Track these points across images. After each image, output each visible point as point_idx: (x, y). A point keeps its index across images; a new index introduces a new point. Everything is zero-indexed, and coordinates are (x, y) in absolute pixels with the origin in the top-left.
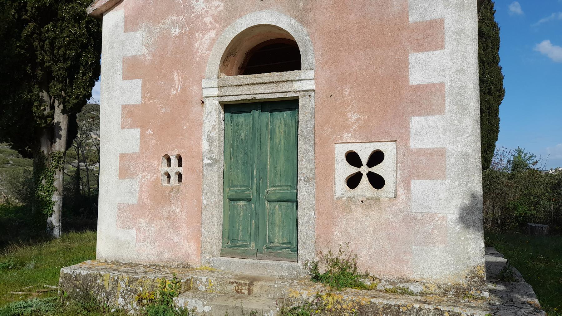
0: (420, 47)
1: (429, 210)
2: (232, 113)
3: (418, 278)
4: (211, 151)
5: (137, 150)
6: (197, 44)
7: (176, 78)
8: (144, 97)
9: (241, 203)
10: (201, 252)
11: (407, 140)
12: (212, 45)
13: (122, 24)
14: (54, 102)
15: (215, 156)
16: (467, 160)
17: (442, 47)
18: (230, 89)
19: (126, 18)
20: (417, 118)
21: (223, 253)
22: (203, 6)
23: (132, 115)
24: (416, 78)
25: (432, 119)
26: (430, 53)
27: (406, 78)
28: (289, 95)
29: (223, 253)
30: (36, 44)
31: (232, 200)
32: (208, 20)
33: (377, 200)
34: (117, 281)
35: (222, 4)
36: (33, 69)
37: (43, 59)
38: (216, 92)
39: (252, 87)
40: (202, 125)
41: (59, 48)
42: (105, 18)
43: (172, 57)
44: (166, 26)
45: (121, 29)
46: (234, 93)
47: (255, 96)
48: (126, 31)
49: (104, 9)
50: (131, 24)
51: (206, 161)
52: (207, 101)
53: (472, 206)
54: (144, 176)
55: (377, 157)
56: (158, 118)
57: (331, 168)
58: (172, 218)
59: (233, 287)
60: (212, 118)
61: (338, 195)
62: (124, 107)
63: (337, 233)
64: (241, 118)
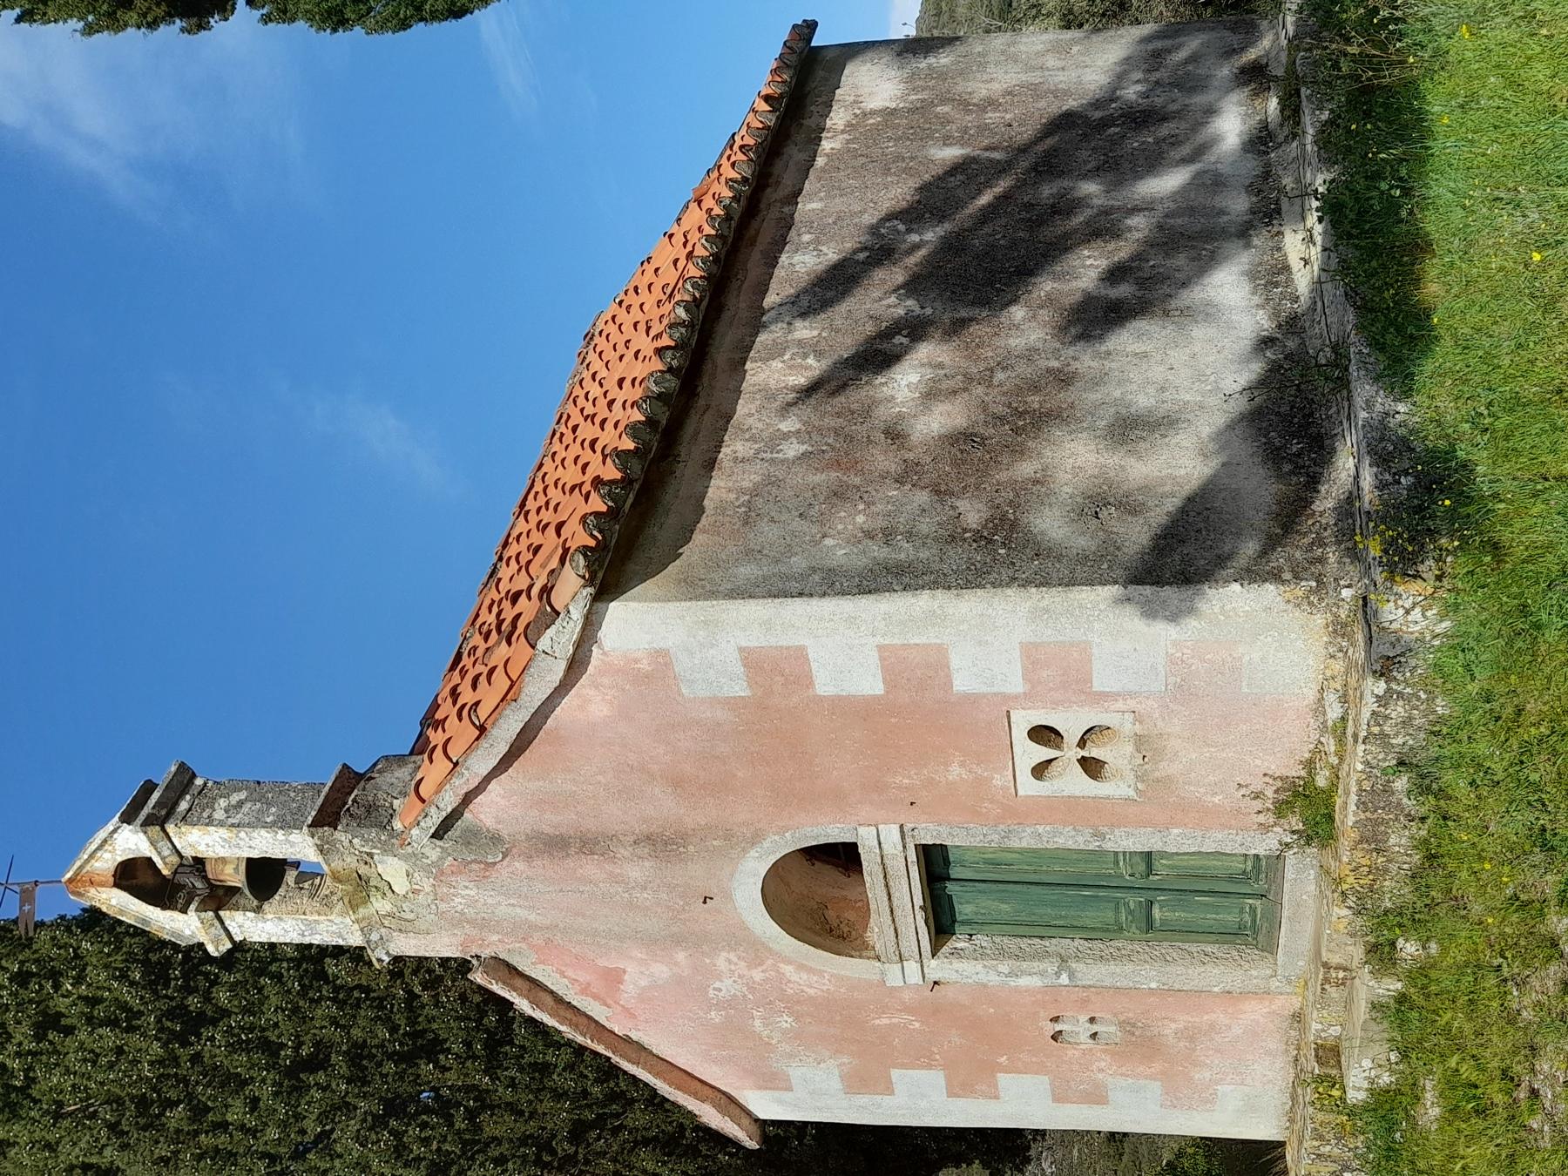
0: (804, 679)
1: (1160, 668)
2: (954, 921)
4: (1042, 974)
6: (811, 992)
8: (929, 1067)
9: (1157, 913)
11: (1006, 698)
13: (777, 1094)
18: (904, 944)
19: (760, 1088)
20: (955, 683)
21: (1270, 948)
24: (870, 683)
25: (955, 661)
26: (814, 666)
28: (912, 857)
31: (1150, 925)
32: (757, 975)
34: (1318, 1155)
35: (724, 954)
38: (912, 967)
39: (897, 912)
40: (985, 986)
42: (762, 1116)
45: (787, 1096)
47: (917, 907)
48: (790, 1089)
49: (746, 1121)
50: (773, 1081)
52: (933, 975)
54: (1101, 1070)
55: (1044, 734)
56: (981, 1044)
58: (1191, 1036)
59: (1332, 991)
60: (966, 969)
61: (1132, 793)
62: (951, 1094)
64: (964, 910)
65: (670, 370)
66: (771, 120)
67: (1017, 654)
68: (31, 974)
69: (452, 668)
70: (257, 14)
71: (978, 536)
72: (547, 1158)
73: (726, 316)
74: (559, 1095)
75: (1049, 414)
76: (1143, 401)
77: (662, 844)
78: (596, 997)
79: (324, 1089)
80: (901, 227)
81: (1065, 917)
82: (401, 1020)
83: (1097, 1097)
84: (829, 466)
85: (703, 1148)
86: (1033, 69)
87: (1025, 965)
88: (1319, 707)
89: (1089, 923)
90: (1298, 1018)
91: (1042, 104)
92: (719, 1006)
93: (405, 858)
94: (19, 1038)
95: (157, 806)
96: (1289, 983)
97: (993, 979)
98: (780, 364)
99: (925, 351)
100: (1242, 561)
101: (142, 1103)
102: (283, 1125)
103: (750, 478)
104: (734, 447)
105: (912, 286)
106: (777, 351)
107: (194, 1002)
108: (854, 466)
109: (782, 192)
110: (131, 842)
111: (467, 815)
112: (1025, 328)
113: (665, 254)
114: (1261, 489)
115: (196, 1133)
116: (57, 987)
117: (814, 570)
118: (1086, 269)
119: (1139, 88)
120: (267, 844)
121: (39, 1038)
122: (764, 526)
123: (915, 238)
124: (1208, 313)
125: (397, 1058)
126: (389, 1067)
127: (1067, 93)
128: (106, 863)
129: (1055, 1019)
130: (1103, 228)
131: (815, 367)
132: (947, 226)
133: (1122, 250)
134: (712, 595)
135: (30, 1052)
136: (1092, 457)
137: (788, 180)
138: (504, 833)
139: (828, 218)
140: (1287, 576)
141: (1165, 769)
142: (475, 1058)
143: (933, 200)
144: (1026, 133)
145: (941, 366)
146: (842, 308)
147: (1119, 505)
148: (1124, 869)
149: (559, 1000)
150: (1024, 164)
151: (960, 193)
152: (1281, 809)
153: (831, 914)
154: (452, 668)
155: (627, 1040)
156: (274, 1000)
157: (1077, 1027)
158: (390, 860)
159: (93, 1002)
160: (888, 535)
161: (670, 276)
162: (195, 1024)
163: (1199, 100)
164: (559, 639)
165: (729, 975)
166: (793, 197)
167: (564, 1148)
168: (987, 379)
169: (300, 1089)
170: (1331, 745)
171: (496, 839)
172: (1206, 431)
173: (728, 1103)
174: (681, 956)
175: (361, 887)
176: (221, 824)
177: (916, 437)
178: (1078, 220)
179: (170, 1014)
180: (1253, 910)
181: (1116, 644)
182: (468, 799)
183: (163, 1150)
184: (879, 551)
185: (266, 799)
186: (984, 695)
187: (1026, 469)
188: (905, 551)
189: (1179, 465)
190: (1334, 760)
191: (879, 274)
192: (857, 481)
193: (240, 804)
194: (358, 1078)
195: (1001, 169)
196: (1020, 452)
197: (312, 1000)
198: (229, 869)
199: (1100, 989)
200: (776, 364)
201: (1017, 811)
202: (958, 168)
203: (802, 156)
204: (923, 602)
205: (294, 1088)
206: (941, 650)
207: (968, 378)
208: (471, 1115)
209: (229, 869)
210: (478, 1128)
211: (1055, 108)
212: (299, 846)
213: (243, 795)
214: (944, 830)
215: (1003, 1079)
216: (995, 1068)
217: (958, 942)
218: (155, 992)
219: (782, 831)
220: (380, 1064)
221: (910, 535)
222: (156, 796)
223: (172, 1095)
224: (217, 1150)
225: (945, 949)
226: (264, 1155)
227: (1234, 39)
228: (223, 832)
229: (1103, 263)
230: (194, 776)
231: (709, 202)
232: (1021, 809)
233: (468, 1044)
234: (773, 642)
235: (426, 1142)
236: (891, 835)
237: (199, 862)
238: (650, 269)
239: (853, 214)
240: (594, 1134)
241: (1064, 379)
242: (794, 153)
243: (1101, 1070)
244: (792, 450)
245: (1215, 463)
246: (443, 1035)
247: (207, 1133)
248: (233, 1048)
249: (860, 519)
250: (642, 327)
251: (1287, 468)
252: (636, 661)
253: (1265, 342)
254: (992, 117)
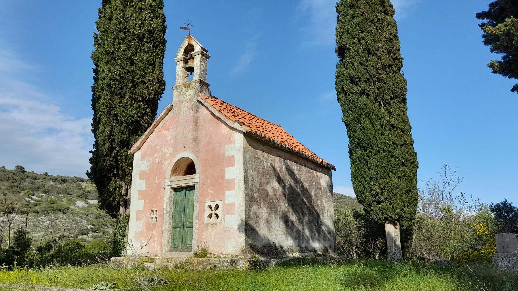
4: (167, 208)
5: (142, 209)
8: (146, 187)
9: (178, 229)
11: (224, 200)
12: (169, 165)
15: (168, 210)
17: (234, 166)
21: (171, 250)
23: (142, 195)
24: (228, 177)
25: (231, 191)
27: (224, 176)
28: (192, 184)
29: (171, 250)
30: (119, 158)
31: (175, 228)
32: (168, 155)
36: (118, 171)
38: (169, 184)
41: (129, 160)
45: (140, 159)
48: (141, 160)
50: (143, 157)
51: (165, 212)
52: (166, 188)
53: (242, 223)
55: (217, 207)
56: (151, 196)
57: (203, 212)
60: (168, 194)
62: (139, 191)
64: (179, 193)
68: (152, 7)
70: (338, 62)
71: (252, 196)
74: (123, 112)
76: (272, 225)
77: (196, 140)
78: (163, 125)
82: (140, 80)
83: (138, 219)
88: (222, 254)
89: (176, 216)
92: (161, 148)
93: (194, 95)
95: (204, 54)
97: (166, 199)
98: (278, 162)
99: (280, 189)
101: (125, 28)
102: (119, 56)
103: (261, 158)
104: (266, 155)
105: (291, 186)
106: (281, 162)
109: (306, 164)
110: (198, 49)
112: (284, 206)
113: (294, 141)
114: (259, 244)
115: (118, 39)
116: (149, 13)
118: (293, 217)
120: (197, 71)
121: (139, 9)
124: (286, 238)
129: (156, 211)
130: (300, 220)
131: (278, 169)
132: (300, 193)
134: (244, 151)
137: (308, 165)
139: (302, 172)
141: (210, 229)
142: (132, 95)
143: (305, 191)
144: (316, 208)
146: (287, 174)
149: (163, 119)
152: (202, 249)
153: (178, 169)
155: (153, 131)
156: (146, 56)
158: (193, 92)
159: (145, 19)
161: (291, 143)
162: (141, 40)
164: (237, 126)
165: (167, 150)
166: (305, 166)
167: (113, 112)
168: (276, 199)
169: (127, 60)
170: (216, 256)
171: (197, 111)
172: (268, 236)
173: (139, 149)
175: (188, 86)
177: (267, 186)
181: (234, 219)
182: (205, 106)
183: (115, 32)
184: (250, 179)
185: (204, 71)
187: (262, 205)
188: (250, 183)
189: (262, 231)
191: (293, 181)
194: (128, 72)
196: (265, 204)
200: (279, 162)
201: (202, 202)
202: (310, 196)
204: (243, 186)
205: (127, 59)
206: (234, 189)
207: (276, 195)
208: (120, 94)
211: (320, 214)
212: (196, 76)
215: (143, 201)
217: (173, 192)
221: (252, 184)
224: (115, 42)
226: (113, 51)
227: (332, 248)
231: (304, 150)
232: (201, 204)
233: (135, 94)
234: (236, 161)
235: (115, 85)
236: (197, 180)
237: (193, 58)
238: (291, 138)
241: (276, 212)
242: (313, 166)
244: (265, 165)
245: (263, 237)
248: (136, 47)
253: (282, 247)
254: (319, 202)
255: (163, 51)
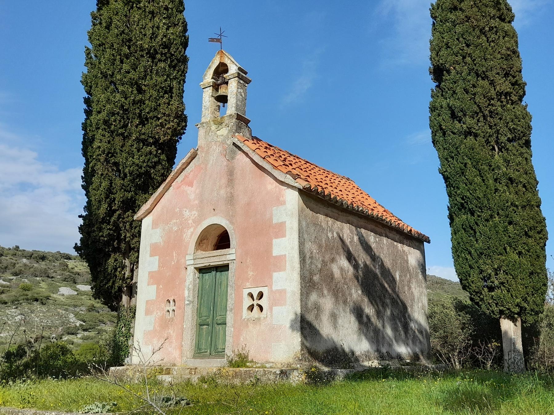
0: (277, 237)
3: (273, 361)
4: (189, 297)
6: (185, 236)
7: (174, 255)
8: (159, 266)
9: (205, 327)
10: (182, 355)
11: (271, 286)
12: (192, 236)
13: (151, 225)
14: (133, 267)
15: (191, 299)
16: (295, 295)
18: (199, 260)
19: (153, 221)
21: (194, 357)
22: (188, 214)
23: (154, 278)
24: (276, 252)
25: (282, 273)
26: (281, 239)
27: (271, 252)
28: (225, 262)
29: (194, 357)
30: (121, 225)
31: (201, 325)
32: (190, 222)
33: (259, 319)
36: (119, 243)
37: (125, 236)
38: (192, 262)
39: (209, 258)
43: (173, 243)
44: (171, 226)
45: (150, 227)
46: (218, 260)
48: (152, 228)
49: (142, 216)
50: (155, 225)
51: (187, 302)
52: (188, 268)
53: (296, 319)
54: (157, 313)
55: (261, 295)
56: (166, 280)
59: (188, 371)
60: (190, 277)
61: (244, 318)
62: (149, 273)
63: (242, 339)
64: (207, 276)
65: (348, 206)
66: (405, 231)
67: (283, 288)
68: (168, 10)
69: (269, 145)
71: (311, 279)
72: (110, 155)
73: (359, 219)
74: (127, 159)
75: (337, 298)
76: (340, 321)
77: (231, 200)
78: (184, 179)
79: (132, 92)
80: (380, 264)
81: (204, 302)
82: (151, 114)
83: (148, 312)
84: (326, 244)
85: (108, 200)
86: (418, 300)
87: (191, 292)
89: (202, 309)
90: (174, 365)
91: (409, 301)
94: (149, 6)
96: (185, 362)
97: (187, 283)
98: (348, 232)
99: (351, 269)
100: (305, 342)
101: (130, 40)
102: (121, 80)
105: (366, 265)
106: (351, 231)
107: (158, 56)
108: (326, 250)
109: (388, 233)
110: (233, 69)
111: (240, 152)
112: (356, 294)
113: (371, 201)
114: (321, 349)
115: (120, 55)
116: (164, 18)
117: (304, 240)
118: (369, 310)
119: (413, 327)
122: (314, 228)
123: (377, 267)
124: (360, 340)
125: (140, 114)
126: (138, 111)
127: (412, 308)
128: (227, 61)
129: (174, 301)
130: (379, 314)
132: (380, 275)
133: (374, 319)
134: (299, 216)
135: (145, 9)
136: (328, 308)
137: (391, 235)
138: (234, 160)
140: (302, 352)
141: (251, 326)
142: (140, 135)
143: (387, 273)
144: (402, 297)
145: (348, 272)
147: (317, 314)
148: (218, 318)
149: (183, 169)
150: (395, 296)
151: (388, 279)
152: (240, 355)
153: (205, 241)
154: (269, 145)
155: (170, 186)
157: (171, 307)
159: (158, 28)
160: (311, 258)
162: (153, 57)
163: (410, 342)
164: (289, 179)
165: (190, 214)
166: (387, 236)
167: (112, 160)
169: (132, 85)
170: (259, 365)
171: (233, 158)
173: (149, 212)
174: (197, 202)
175: (219, 123)
176: (237, 91)
178: (381, 308)
179: (155, 50)
180: (206, 352)
181: (284, 312)
182: (244, 152)
183: (115, 46)
184: (308, 255)
185: (243, 102)
186: (272, 280)
187: (325, 292)
188: (308, 261)
189: (326, 329)
190: (255, 366)
191: (369, 258)
192: (323, 251)
193: (241, 95)
195: (394, 290)
196: (329, 291)
197: (159, 90)
198: (224, 90)
199: (184, 312)
200: (348, 231)
201: (239, 289)
203: (397, 239)
205: (132, 84)
206: (285, 270)
208: (122, 134)
209: (224, 90)
210: (118, 135)
211: (408, 305)
212: (231, 108)
213: (243, 96)
214: (233, 271)
216: (158, 285)
217: (197, 274)
218: (160, 45)
219: (234, 230)
220: (138, 108)
221: (311, 263)
222: (244, 75)
223: (132, 49)
224: (115, 60)
225: (196, 271)
226: (113, 73)
227: (425, 353)
228: (236, 91)
229: (371, 314)
230: (248, 84)
231: (385, 214)
232: (238, 291)
233: (144, 134)
235: (115, 121)
237: (227, 83)
238: (366, 197)
239: (383, 251)
240: (115, 169)
241: (345, 302)
242: (397, 237)
243: (157, 313)
244: (330, 235)
245: (326, 338)
246: (146, 126)
247: (120, 58)
248: (145, 67)
249: (315, 251)
250: (353, 196)
251: (325, 355)
252: (283, 197)
253: (353, 353)
254: (406, 288)
255: (184, 73)
